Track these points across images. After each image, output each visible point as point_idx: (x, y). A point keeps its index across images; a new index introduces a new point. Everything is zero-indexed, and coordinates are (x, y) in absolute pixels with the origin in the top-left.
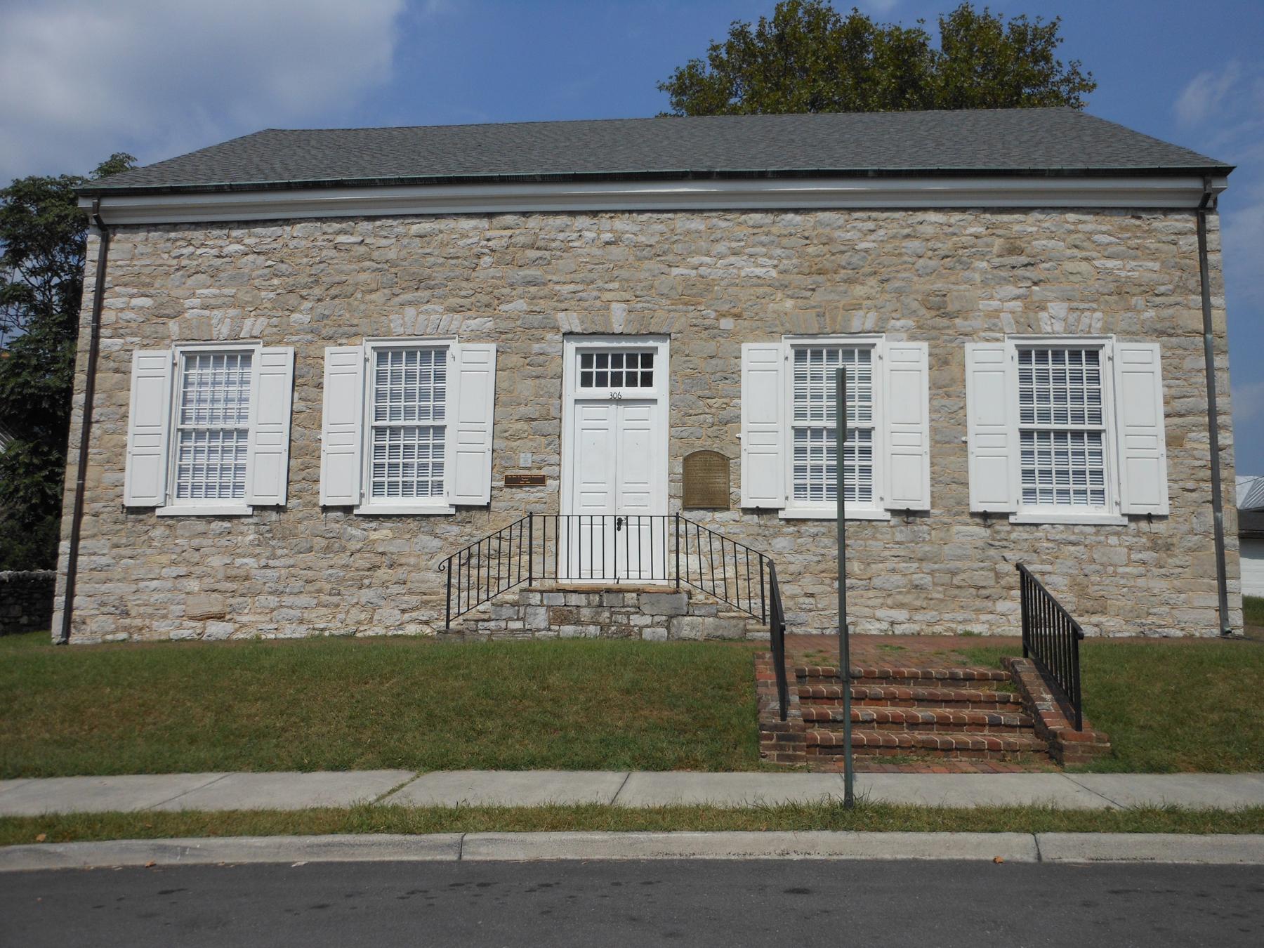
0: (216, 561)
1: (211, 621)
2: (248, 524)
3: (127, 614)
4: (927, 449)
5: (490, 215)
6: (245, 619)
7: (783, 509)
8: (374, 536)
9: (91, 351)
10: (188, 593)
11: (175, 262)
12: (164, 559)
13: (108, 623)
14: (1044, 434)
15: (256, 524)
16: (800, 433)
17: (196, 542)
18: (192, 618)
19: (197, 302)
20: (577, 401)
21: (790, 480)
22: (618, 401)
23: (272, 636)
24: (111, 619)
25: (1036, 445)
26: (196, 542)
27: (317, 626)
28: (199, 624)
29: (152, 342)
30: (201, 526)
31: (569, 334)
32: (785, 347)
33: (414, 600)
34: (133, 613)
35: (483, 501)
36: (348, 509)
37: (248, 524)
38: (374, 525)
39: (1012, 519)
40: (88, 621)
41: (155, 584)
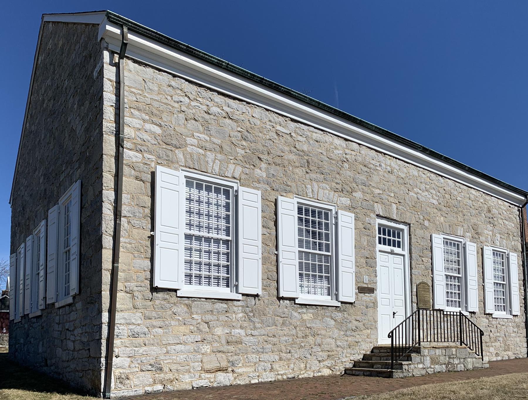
0: (219, 331)
1: (219, 373)
2: (238, 306)
3: (161, 369)
4: (260, 256)
5: (174, 76)
6: (240, 370)
7: (297, 298)
8: (305, 317)
9: (115, 157)
10: (203, 354)
11: (176, 105)
12: (183, 329)
13: (148, 377)
14: (199, 238)
15: (242, 306)
16: (188, 237)
17: (208, 317)
18: (208, 371)
19: (195, 142)
20: (380, 251)
21: (183, 270)
22: (392, 253)
23: (256, 381)
24: (148, 375)
25: (195, 245)
26: (208, 317)
27: (279, 373)
28: (212, 375)
29: (165, 162)
30: (208, 306)
31: (378, 216)
32: (181, 175)
33: (325, 354)
34: (165, 369)
35: (352, 301)
36: (293, 299)
37: (238, 306)
38: (304, 310)
39: (179, 294)
40: (131, 376)
41: (178, 347)
